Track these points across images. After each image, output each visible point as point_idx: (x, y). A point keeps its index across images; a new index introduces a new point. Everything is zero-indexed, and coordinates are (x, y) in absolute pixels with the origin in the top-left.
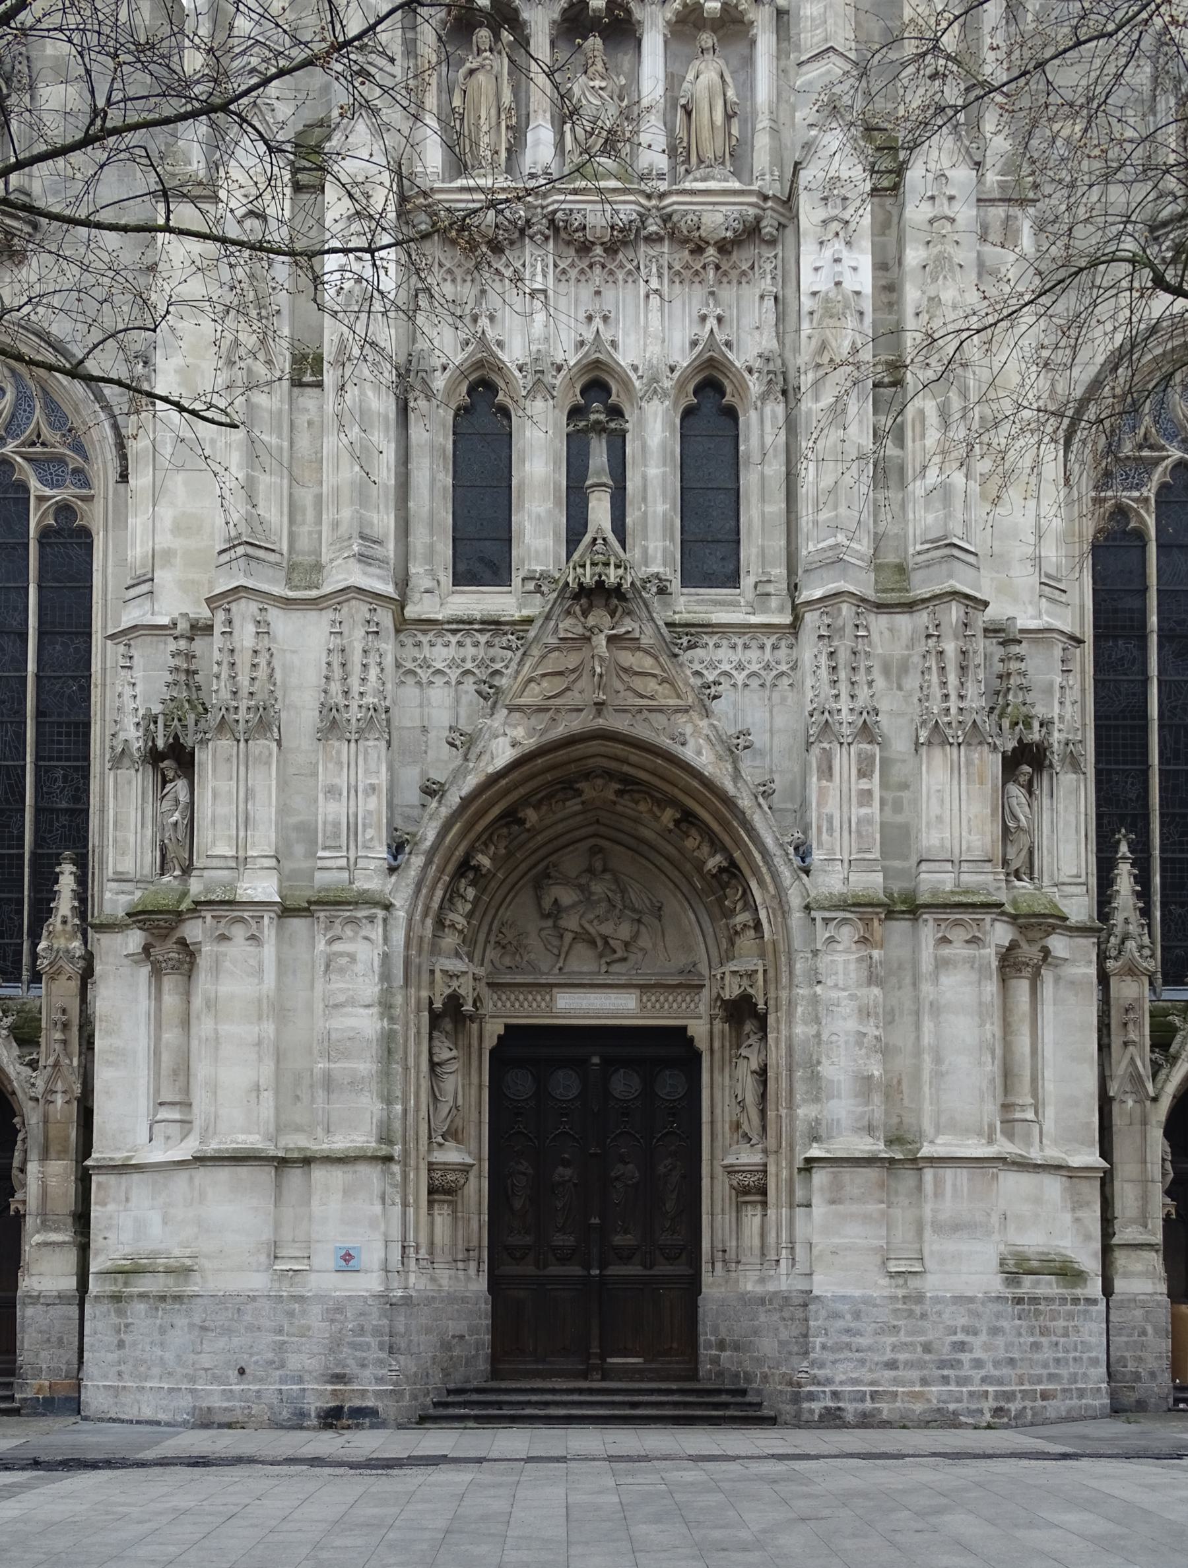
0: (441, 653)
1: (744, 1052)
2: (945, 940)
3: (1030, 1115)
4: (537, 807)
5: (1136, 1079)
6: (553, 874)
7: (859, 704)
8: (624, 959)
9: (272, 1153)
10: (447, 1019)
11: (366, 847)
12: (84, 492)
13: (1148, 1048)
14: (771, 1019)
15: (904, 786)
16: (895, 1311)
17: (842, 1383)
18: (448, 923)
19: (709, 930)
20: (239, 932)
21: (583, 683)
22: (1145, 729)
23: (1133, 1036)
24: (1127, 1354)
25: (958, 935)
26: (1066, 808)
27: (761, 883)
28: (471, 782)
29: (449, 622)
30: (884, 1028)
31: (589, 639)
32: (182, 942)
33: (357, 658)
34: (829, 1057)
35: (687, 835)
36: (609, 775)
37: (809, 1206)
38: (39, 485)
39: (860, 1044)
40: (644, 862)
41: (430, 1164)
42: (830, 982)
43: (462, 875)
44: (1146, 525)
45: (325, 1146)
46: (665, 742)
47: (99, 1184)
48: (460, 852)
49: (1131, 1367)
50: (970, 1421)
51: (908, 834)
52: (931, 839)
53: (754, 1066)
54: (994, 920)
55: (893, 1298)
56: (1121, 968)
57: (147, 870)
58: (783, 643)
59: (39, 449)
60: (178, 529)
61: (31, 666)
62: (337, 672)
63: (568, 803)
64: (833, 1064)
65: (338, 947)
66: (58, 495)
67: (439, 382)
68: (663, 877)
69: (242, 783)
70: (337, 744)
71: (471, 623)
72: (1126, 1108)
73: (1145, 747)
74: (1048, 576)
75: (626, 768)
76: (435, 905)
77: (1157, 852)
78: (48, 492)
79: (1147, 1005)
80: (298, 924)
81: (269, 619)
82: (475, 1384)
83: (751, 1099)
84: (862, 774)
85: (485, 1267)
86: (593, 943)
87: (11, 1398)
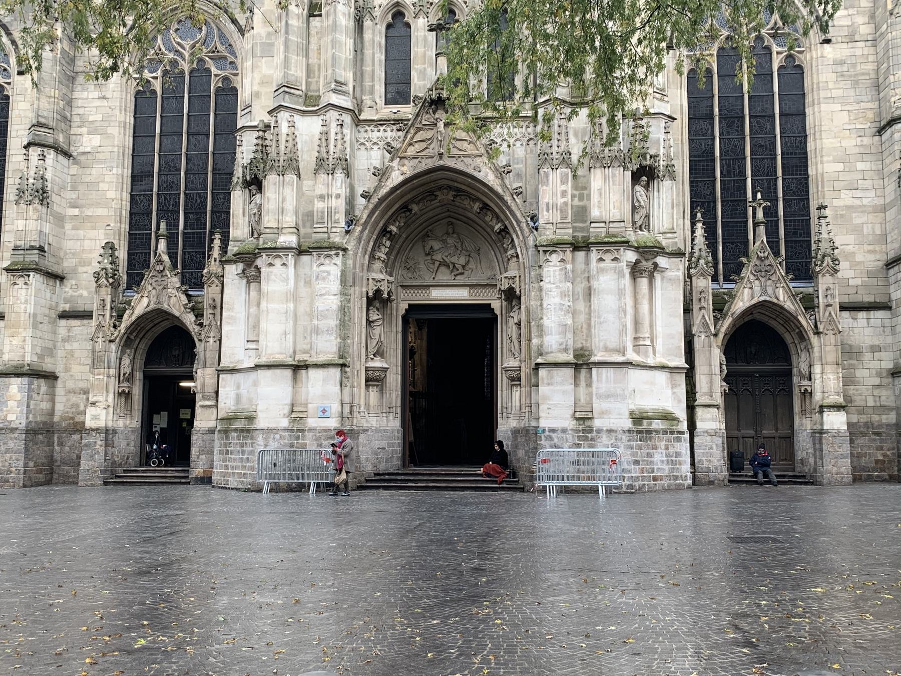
0: (375, 134)
1: (512, 314)
2: (601, 260)
3: (648, 342)
4: (418, 203)
5: (705, 325)
6: (430, 235)
7: (560, 150)
8: (462, 274)
9: (290, 363)
10: (377, 301)
11: (335, 222)
12: (235, 72)
13: (711, 311)
14: (523, 298)
15: (585, 188)
16: (578, 437)
17: (554, 472)
18: (377, 257)
19: (500, 259)
20: (278, 262)
21: (435, 145)
22: (713, 161)
23: (704, 305)
24: (704, 459)
25: (608, 257)
26: (667, 197)
27: (517, 236)
28: (384, 191)
29: (379, 121)
30: (573, 302)
31: (436, 124)
32: (256, 267)
33: (332, 136)
34: (547, 316)
35: (486, 215)
36: (450, 188)
37: (538, 386)
38: (216, 70)
39: (561, 310)
40: (470, 228)
41: (366, 368)
42: (547, 281)
43: (384, 236)
44: (711, 65)
45: (315, 360)
46: (470, 171)
47: (223, 378)
48: (381, 224)
49: (706, 464)
50: (616, 491)
51: (586, 210)
52: (595, 213)
53: (516, 321)
54: (625, 249)
55: (578, 431)
56: (697, 272)
57: (246, 236)
58: (531, 125)
59: (216, 54)
60: (262, 83)
61: (211, 149)
62: (324, 144)
63: (432, 203)
64: (548, 319)
65: (322, 268)
66: (223, 73)
67: (377, 13)
68: (480, 236)
69: (281, 194)
70: (323, 176)
71: (389, 121)
72: (699, 342)
73: (714, 169)
74: (657, 89)
75: (456, 184)
76: (370, 249)
77: (720, 218)
78: (220, 72)
79: (711, 291)
80: (305, 259)
81: (295, 120)
82: (391, 471)
83: (514, 337)
84: (563, 183)
85: (399, 416)
86: (448, 266)
87: (188, 477)
